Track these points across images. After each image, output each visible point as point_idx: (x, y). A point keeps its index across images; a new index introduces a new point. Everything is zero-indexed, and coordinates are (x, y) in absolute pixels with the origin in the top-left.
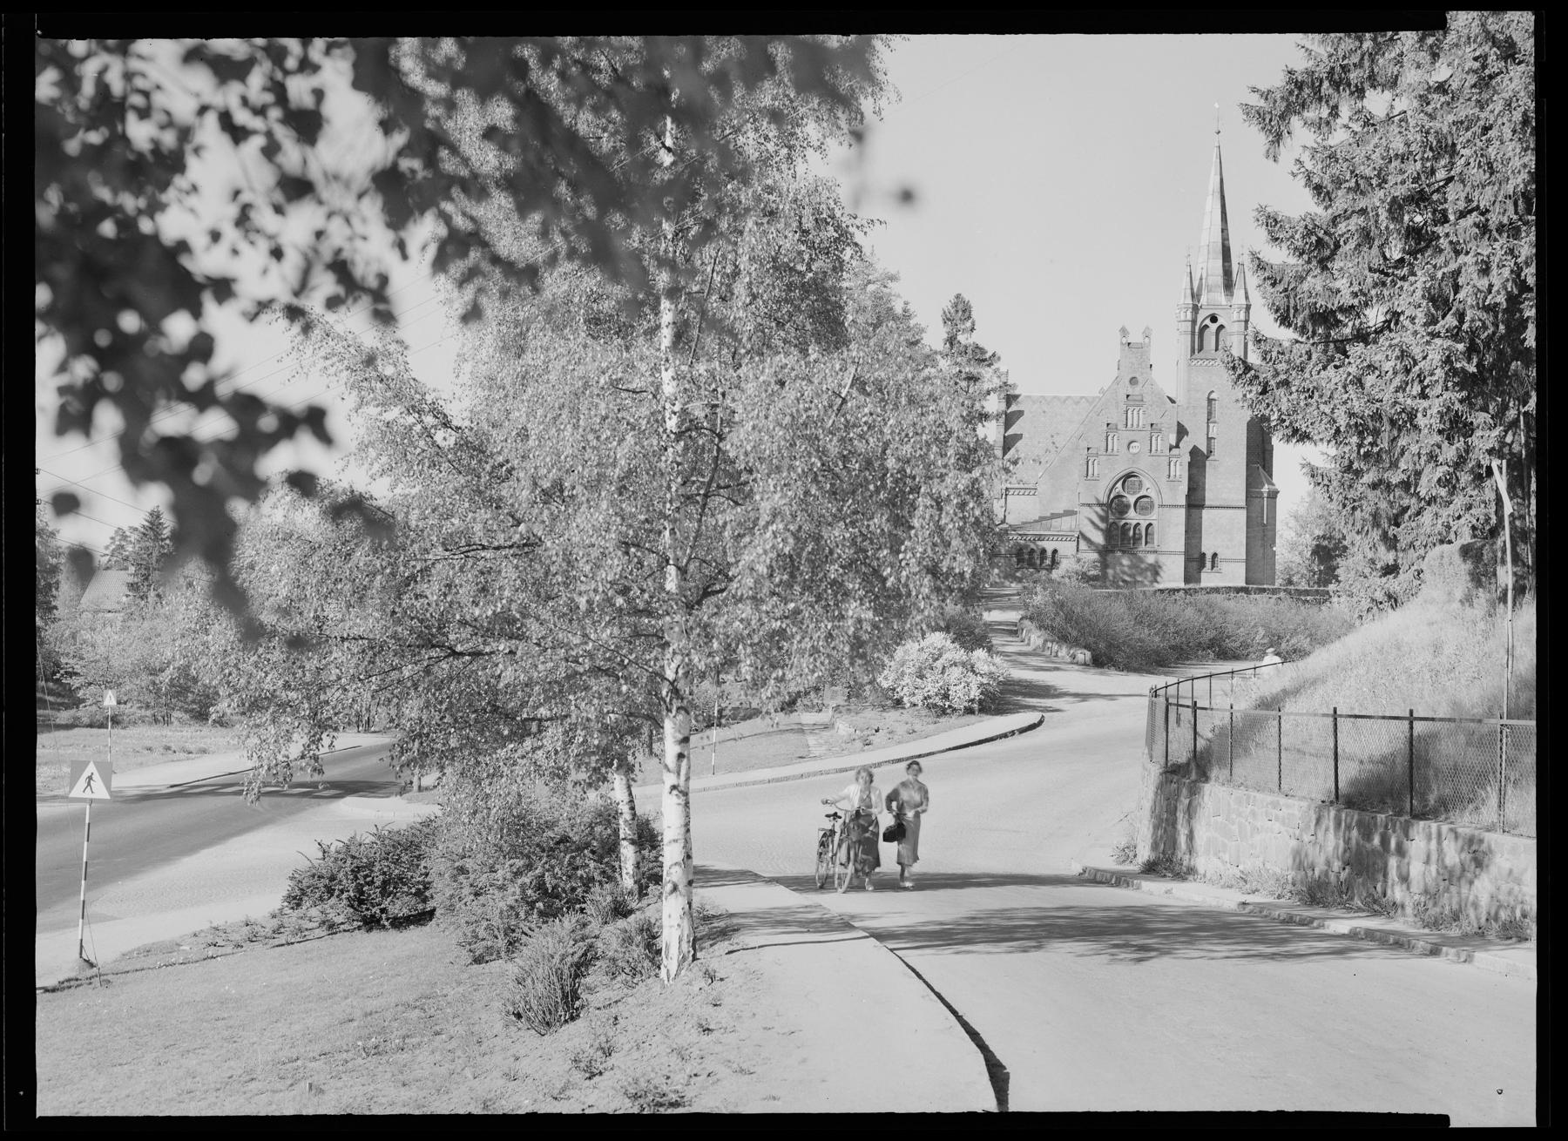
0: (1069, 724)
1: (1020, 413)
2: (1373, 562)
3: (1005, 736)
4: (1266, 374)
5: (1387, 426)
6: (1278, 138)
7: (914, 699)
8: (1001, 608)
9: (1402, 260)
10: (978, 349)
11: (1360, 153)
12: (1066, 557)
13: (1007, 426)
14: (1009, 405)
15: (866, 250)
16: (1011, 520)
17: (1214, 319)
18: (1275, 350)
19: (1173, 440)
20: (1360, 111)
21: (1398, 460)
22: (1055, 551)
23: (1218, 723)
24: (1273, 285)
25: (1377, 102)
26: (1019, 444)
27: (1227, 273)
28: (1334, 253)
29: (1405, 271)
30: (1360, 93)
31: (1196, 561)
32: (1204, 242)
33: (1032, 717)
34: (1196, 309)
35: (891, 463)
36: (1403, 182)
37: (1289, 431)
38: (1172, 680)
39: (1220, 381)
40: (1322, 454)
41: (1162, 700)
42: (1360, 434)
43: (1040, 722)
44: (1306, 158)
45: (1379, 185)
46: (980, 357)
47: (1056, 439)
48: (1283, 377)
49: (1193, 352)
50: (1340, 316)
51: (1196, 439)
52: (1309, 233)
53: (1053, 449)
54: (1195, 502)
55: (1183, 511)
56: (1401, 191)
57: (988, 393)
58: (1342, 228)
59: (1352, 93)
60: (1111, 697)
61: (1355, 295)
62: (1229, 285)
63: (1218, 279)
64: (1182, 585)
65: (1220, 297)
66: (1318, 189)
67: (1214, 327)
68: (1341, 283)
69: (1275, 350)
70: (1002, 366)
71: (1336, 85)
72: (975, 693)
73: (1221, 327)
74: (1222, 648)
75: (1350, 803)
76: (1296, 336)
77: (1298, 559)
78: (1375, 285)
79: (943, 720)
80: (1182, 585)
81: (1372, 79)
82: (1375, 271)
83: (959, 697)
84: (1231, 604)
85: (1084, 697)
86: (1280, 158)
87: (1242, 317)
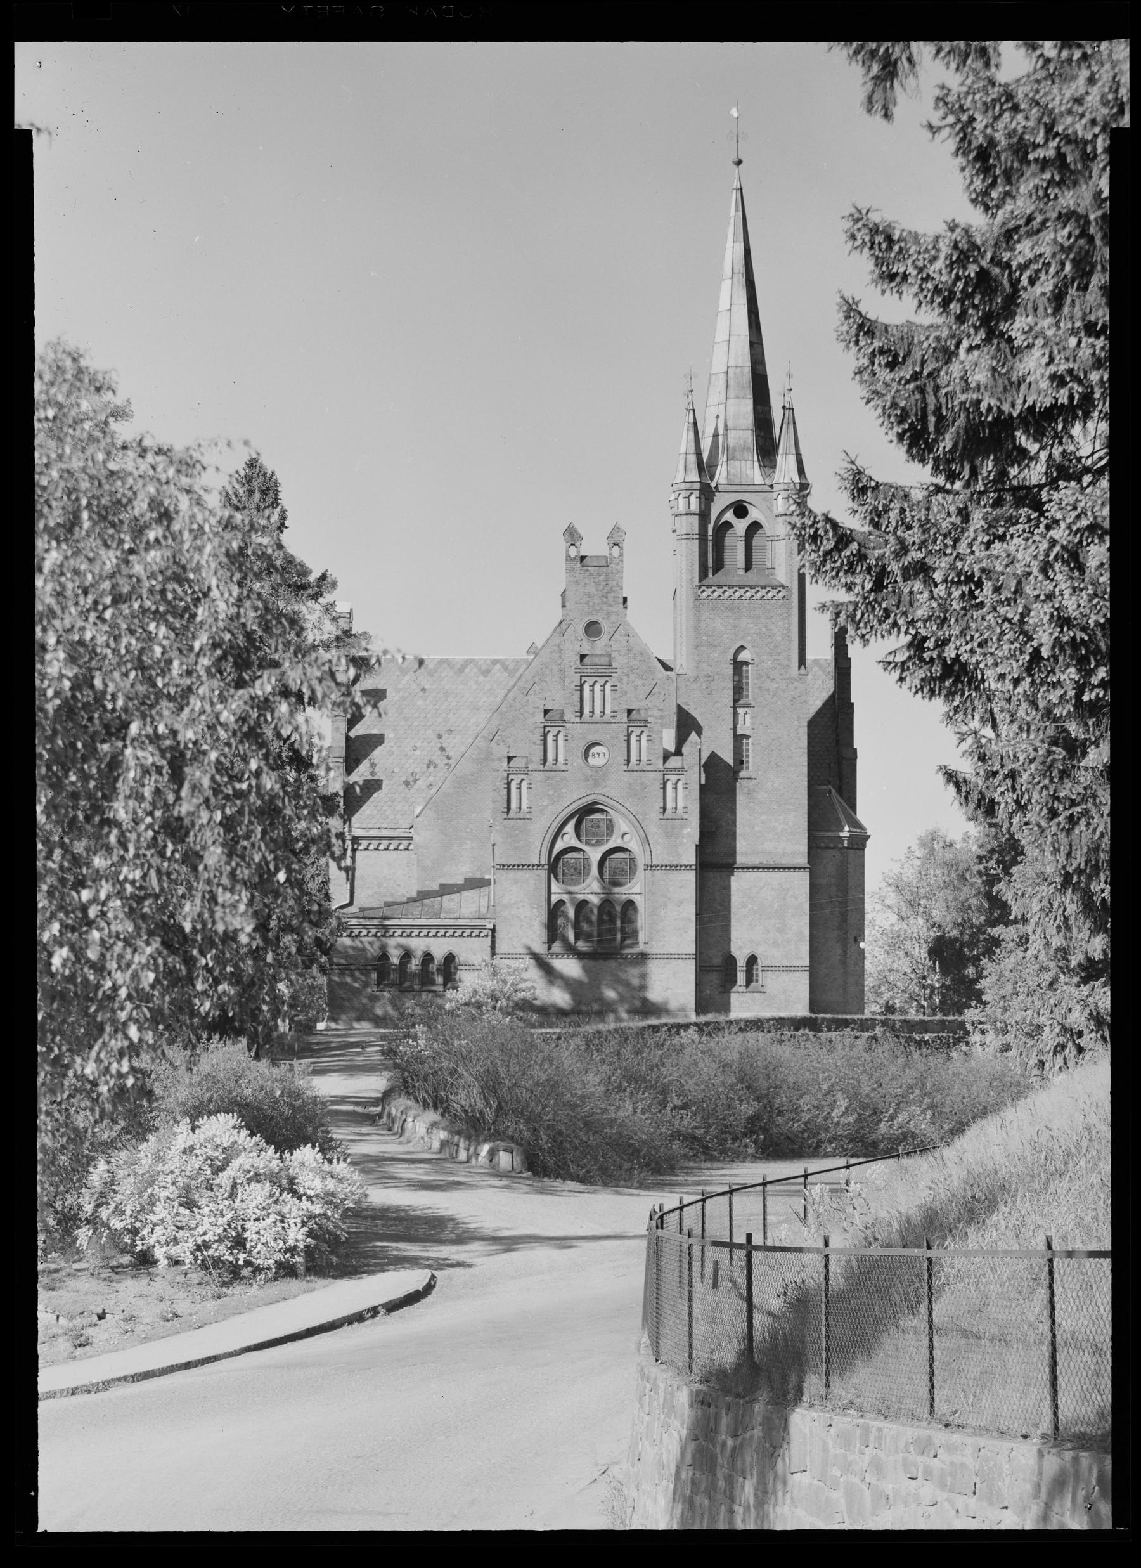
0: (479, 1293)
4: (882, 550)
7: (175, 1251)
8: (351, 1069)
12: (471, 967)
17: (740, 510)
18: (896, 505)
26: (377, 753)
31: (718, 972)
33: (414, 1279)
34: (707, 493)
37: (937, 670)
43: (429, 1288)
47: (446, 742)
48: (915, 555)
49: (703, 574)
50: (1021, 438)
51: (716, 740)
53: (441, 762)
54: (715, 861)
55: (690, 877)
58: (1025, 249)
60: (563, 1242)
61: (1058, 380)
62: (767, 450)
63: (744, 434)
64: (693, 1018)
65: (752, 470)
66: (982, 158)
67: (741, 526)
69: (896, 505)
70: (341, 600)
72: (297, 1235)
73: (755, 526)
74: (776, 1134)
79: (237, 1291)
80: (693, 1018)
84: (785, 1052)
85: (509, 1243)
86: (896, 111)
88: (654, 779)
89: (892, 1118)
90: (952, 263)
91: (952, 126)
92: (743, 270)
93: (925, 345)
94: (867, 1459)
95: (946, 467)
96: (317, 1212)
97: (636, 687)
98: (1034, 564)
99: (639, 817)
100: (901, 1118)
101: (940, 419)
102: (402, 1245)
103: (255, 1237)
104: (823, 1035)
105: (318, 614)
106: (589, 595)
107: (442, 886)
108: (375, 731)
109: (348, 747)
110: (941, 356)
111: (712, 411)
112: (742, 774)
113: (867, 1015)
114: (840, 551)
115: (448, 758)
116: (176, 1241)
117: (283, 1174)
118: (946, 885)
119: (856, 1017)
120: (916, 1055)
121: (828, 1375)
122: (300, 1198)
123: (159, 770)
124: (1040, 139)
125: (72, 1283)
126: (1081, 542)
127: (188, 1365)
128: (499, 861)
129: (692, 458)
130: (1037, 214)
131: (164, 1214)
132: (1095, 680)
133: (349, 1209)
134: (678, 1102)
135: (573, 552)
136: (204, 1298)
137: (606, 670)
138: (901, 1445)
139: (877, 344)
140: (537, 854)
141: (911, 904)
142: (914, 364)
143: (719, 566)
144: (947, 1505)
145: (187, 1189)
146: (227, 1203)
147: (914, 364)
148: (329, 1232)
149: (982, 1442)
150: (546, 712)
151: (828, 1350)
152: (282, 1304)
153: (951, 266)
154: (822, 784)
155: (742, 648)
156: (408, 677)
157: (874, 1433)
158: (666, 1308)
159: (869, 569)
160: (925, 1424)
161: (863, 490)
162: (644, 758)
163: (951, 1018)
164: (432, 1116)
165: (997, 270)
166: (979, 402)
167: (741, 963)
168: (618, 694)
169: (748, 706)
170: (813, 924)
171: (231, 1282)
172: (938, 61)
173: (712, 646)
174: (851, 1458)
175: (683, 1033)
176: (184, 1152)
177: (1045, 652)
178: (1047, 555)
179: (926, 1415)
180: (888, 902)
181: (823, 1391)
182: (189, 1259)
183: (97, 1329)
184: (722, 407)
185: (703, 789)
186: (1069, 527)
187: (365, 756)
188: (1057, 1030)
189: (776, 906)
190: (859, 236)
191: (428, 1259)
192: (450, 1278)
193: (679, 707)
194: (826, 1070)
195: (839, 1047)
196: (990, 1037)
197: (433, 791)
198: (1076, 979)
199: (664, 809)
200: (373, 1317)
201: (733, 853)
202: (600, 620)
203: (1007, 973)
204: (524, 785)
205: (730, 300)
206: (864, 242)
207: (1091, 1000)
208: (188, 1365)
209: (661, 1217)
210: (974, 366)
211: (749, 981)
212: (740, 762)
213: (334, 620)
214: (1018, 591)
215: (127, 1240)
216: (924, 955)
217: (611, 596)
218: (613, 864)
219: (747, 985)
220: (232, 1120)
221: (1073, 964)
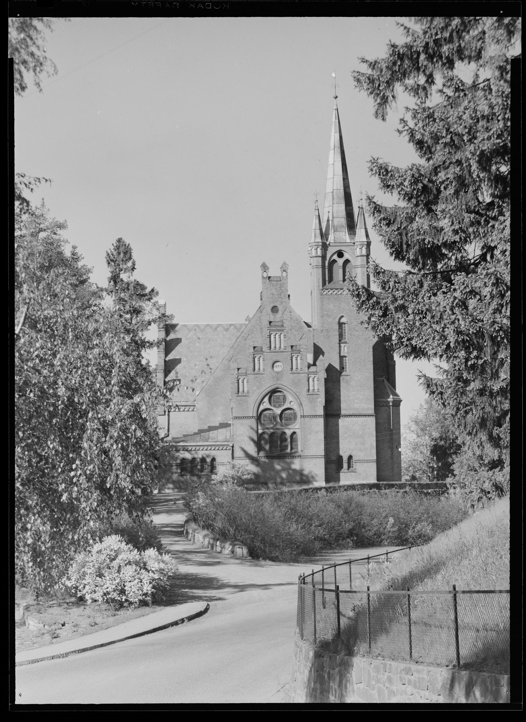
0: (229, 611)
1: (178, 341)
2: (481, 457)
3: (176, 623)
5: (487, 343)
6: (384, 101)
7: (95, 596)
8: (169, 512)
9: (492, 204)
10: (139, 286)
11: (453, 114)
12: (223, 464)
13: (167, 351)
14: (167, 333)
15: (33, 205)
16: (174, 434)
17: (340, 254)
18: (392, 280)
19: (310, 358)
20: (452, 80)
21: (497, 372)
22: (214, 460)
23: (358, 603)
24: (388, 225)
25: (465, 71)
26: (178, 367)
27: (350, 215)
28: (437, 197)
29: (495, 212)
30: (450, 64)
31: (334, 463)
32: (329, 189)
33: (199, 606)
34: (325, 247)
35: (61, 391)
36: (489, 138)
37: (409, 349)
38: (317, 568)
39: (346, 307)
40: (435, 367)
41: (309, 587)
42: (467, 349)
43: (206, 610)
44: (408, 117)
45: (470, 141)
46: (141, 292)
47: (210, 361)
48: (400, 302)
49: (324, 284)
51: (331, 358)
52: (416, 181)
53: (208, 371)
54: (332, 412)
55: (321, 421)
56: (486, 146)
57: (149, 323)
58: (442, 176)
59: (444, 64)
60: (265, 587)
61: (456, 232)
62: (351, 226)
63: (342, 221)
64: (323, 484)
65: (345, 236)
66: (420, 144)
67: (340, 261)
68: (445, 223)
69: (392, 280)
70: (160, 300)
71: (430, 58)
72: (148, 588)
73: (347, 261)
74: (361, 537)
75: (467, 666)
76: (409, 268)
77: (420, 458)
78: (472, 224)
79: (122, 613)
81: (460, 53)
82: (471, 212)
83: (134, 592)
85: (242, 588)
86: (387, 117)
87: (364, 252)
88: (304, 376)
89: (414, 528)
90: (411, 183)
91: (408, 130)
92: (339, 146)
93: (402, 216)
94: (386, 677)
95: (414, 263)
96: (156, 578)
97: (295, 335)
98: (448, 307)
99: (298, 394)
100: (419, 527)
101: (408, 246)
102: (194, 591)
103: (130, 589)
104: (383, 491)
105: (150, 307)
106: (273, 294)
107: (209, 427)
108: (177, 357)
109: (165, 365)
110: (408, 220)
111: (327, 210)
112: (343, 373)
113: (403, 481)
114: (369, 300)
115: (211, 369)
116: (95, 592)
117: (141, 561)
118: (438, 421)
119: (397, 483)
120: (425, 499)
121: (370, 643)
122: (148, 572)
123: (99, 430)
124: (444, 135)
125: (50, 610)
126: (466, 298)
127: (102, 645)
128: (234, 415)
129: (318, 231)
130: (447, 160)
131: (90, 580)
132: (472, 356)
133: (170, 576)
134: (317, 524)
135: (265, 275)
136: (108, 616)
137: (280, 328)
138: (399, 671)
139: (382, 216)
140: (252, 412)
141: (422, 430)
142: (398, 224)
143: (331, 280)
144: (417, 695)
145: (99, 568)
146: (116, 575)
147: (398, 224)
148: (161, 586)
149: (430, 668)
150: (254, 347)
151: (370, 633)
152: (142, 618)
153: (411, 184)
154: (380, 377)
155: (342, 316)
156: (191, 333)
157: (388, 667)
158: (306, 618)
159: (381, 308)
160: (408, 662)
161: (378, 273)
162: (299, 367)
163: (440, 482)
164: (206, 532)
165: (431, 185)
166: (424, 240)
167: (345, 459)
168: (287, 338)
169: (345, 343)
170: (377, 441)
171: (119, 609)
172: (406, 93)
173: (329, 316)
174: (379, 677)
175: (319, 492)
176: (98, 552)
177: (452, 345)
178: (453, 304)
179: (408, 657)
180: (412, 429)
181: (368, 650)
182: (101, 599)
183: (61, 630)
184: (331, 208)
185: (326, 380)
186: (461, 292)
187: (173, 369)
188: (479, 491)
189: (360, 433)
190: (374, 169)
191: (206, 597)
192: (216, 605)
193: (315, 344)
194: (386, 507)
195: (390, 496)
196: (458, 490)
197: (204, 384)
198: (487, 468)
199: (309, 390)
200: (182, 623)
201: (340, 410)
202: (278, 305)
203: (465, 461)
204: (245, 381)
205: (334, 159)
206: (376, 172)
207: (493, 478)
208: (102, 645)
209: (304, 578)
210: (422, 222)
211: (349, 467)
212: (342, 368)
213: (158, 309)
214: (441, 318)
215: (73, 591)
216: (429, 453)
217: (282, 294)
218: (286, 416)
219: (348, 469)
220: (118, 538)
221: (486, 462)
